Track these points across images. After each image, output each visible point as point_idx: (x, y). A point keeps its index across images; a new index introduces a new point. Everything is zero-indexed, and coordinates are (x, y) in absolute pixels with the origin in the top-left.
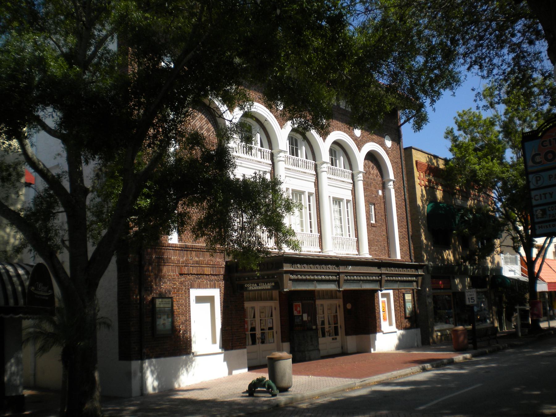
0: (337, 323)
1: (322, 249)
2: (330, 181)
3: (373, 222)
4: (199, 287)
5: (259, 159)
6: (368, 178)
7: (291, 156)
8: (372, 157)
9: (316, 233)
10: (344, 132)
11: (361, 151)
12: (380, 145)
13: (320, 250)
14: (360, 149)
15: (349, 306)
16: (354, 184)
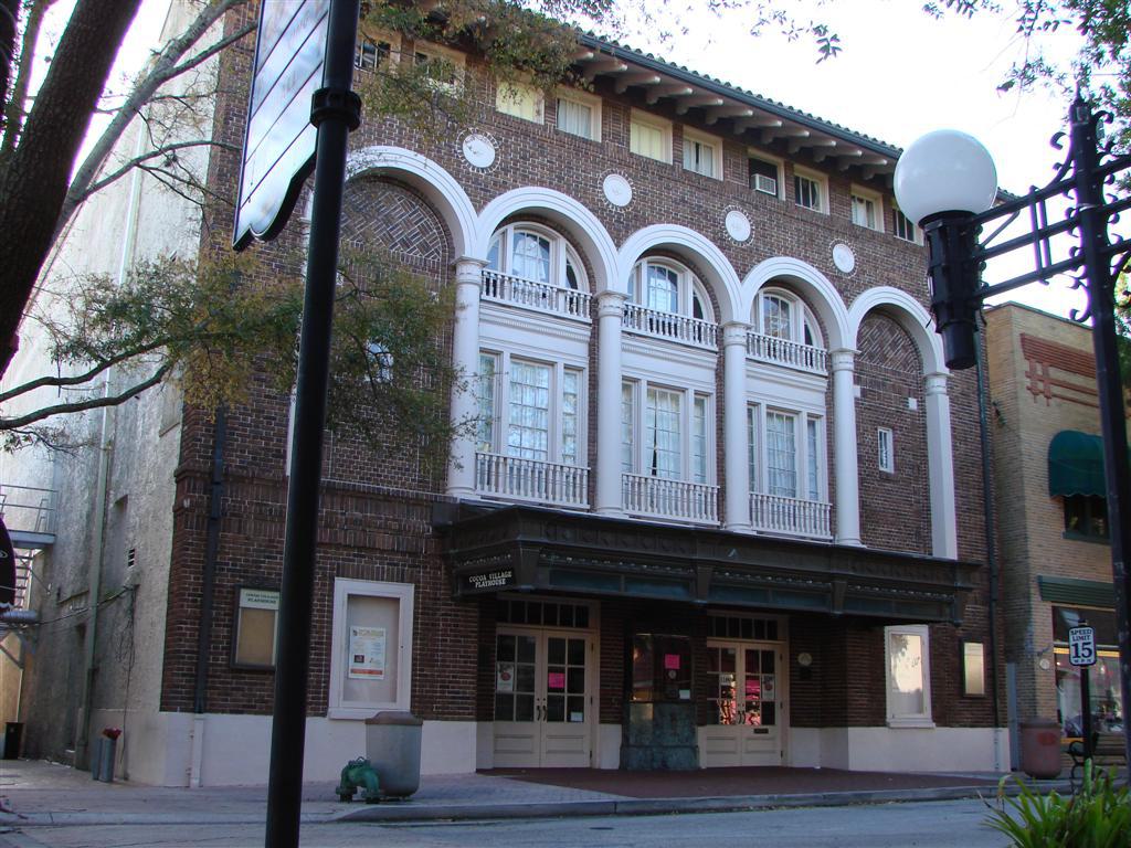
0: (581, 690)
3: (888, 466)
4: (358, 575)
10: (806, 259)
11: (481, 215)
14: (848, 301)
16: (831, 378)
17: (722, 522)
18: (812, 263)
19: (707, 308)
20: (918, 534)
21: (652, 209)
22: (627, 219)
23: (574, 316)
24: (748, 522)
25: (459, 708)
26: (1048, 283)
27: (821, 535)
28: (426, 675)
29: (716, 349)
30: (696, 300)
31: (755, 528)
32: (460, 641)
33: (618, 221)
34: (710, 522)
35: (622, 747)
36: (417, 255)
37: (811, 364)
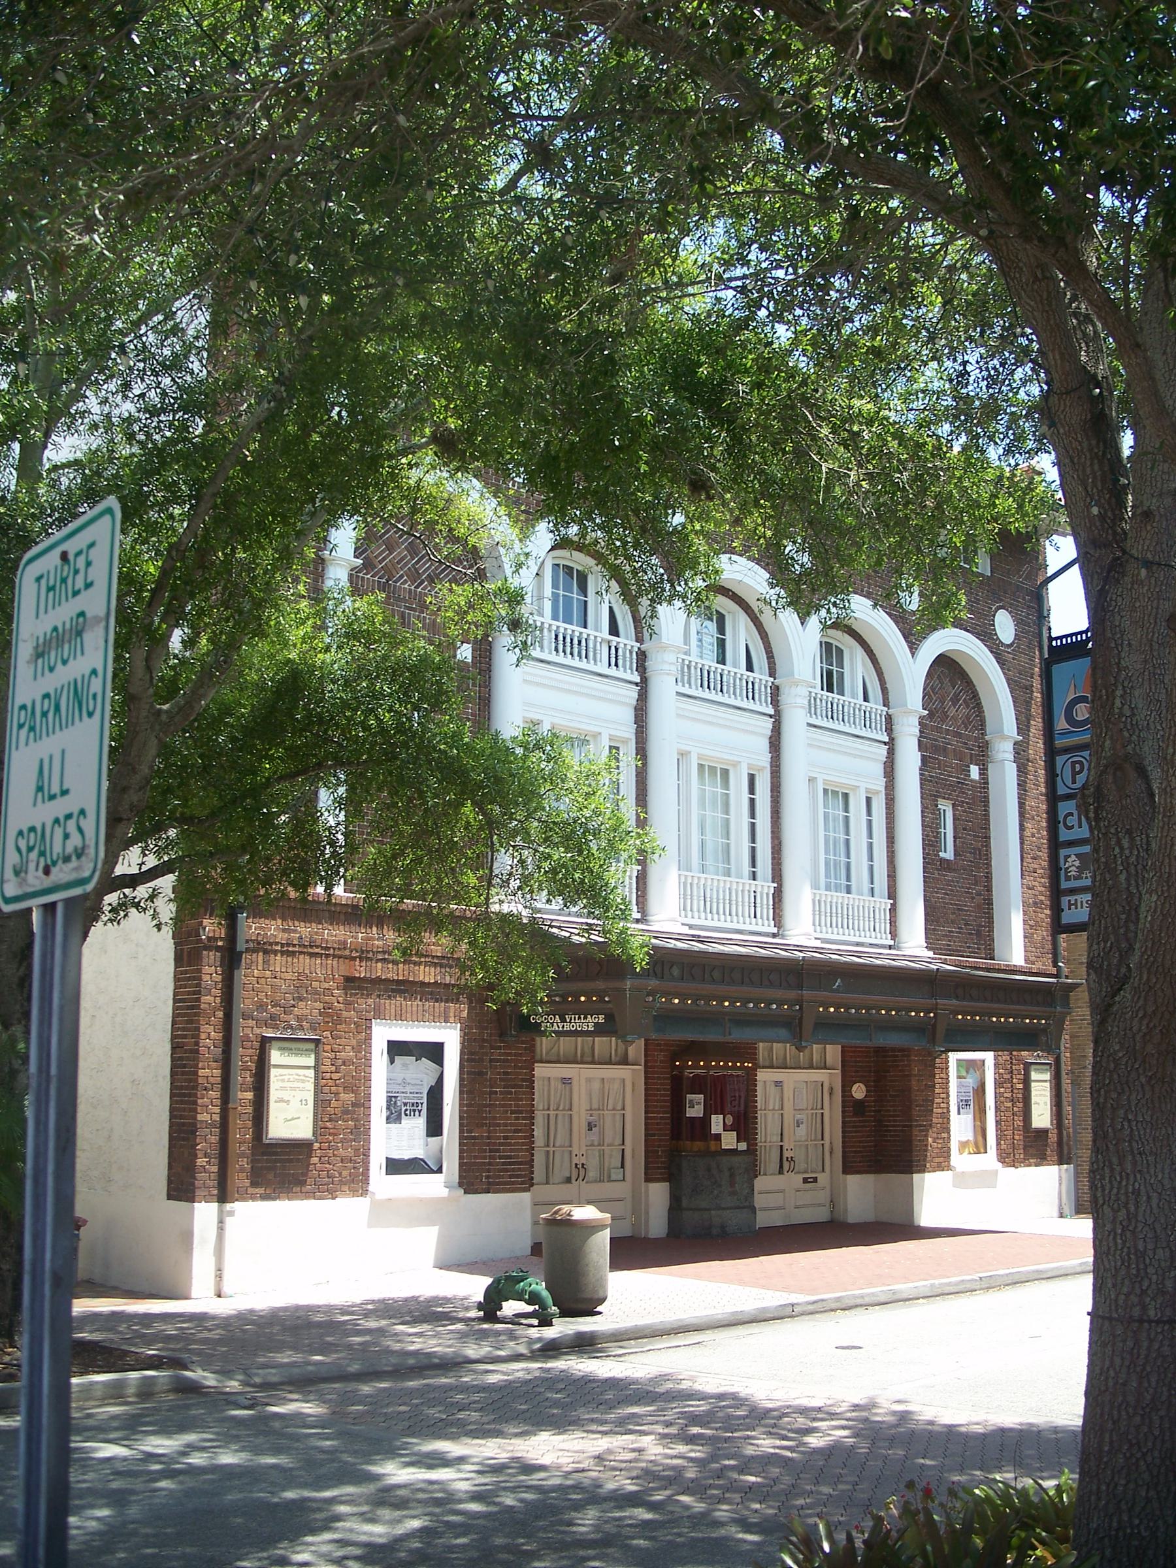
1: (894, 934)
3: (948, 854)
4: (400, 1017)
5: (602, 668)
7: (825, 693)
8: (947, 669)
9: (766, 887)
12: (978, 635)
14: (913, 648)
15: (859, 1091)
16: (891, 745)
19: (760, 659)
20: (979, 934)
23: (750, 705)
24: (811, 929)
25: (511, 1177)
28: (474, 1138)
35: (671, 1209)
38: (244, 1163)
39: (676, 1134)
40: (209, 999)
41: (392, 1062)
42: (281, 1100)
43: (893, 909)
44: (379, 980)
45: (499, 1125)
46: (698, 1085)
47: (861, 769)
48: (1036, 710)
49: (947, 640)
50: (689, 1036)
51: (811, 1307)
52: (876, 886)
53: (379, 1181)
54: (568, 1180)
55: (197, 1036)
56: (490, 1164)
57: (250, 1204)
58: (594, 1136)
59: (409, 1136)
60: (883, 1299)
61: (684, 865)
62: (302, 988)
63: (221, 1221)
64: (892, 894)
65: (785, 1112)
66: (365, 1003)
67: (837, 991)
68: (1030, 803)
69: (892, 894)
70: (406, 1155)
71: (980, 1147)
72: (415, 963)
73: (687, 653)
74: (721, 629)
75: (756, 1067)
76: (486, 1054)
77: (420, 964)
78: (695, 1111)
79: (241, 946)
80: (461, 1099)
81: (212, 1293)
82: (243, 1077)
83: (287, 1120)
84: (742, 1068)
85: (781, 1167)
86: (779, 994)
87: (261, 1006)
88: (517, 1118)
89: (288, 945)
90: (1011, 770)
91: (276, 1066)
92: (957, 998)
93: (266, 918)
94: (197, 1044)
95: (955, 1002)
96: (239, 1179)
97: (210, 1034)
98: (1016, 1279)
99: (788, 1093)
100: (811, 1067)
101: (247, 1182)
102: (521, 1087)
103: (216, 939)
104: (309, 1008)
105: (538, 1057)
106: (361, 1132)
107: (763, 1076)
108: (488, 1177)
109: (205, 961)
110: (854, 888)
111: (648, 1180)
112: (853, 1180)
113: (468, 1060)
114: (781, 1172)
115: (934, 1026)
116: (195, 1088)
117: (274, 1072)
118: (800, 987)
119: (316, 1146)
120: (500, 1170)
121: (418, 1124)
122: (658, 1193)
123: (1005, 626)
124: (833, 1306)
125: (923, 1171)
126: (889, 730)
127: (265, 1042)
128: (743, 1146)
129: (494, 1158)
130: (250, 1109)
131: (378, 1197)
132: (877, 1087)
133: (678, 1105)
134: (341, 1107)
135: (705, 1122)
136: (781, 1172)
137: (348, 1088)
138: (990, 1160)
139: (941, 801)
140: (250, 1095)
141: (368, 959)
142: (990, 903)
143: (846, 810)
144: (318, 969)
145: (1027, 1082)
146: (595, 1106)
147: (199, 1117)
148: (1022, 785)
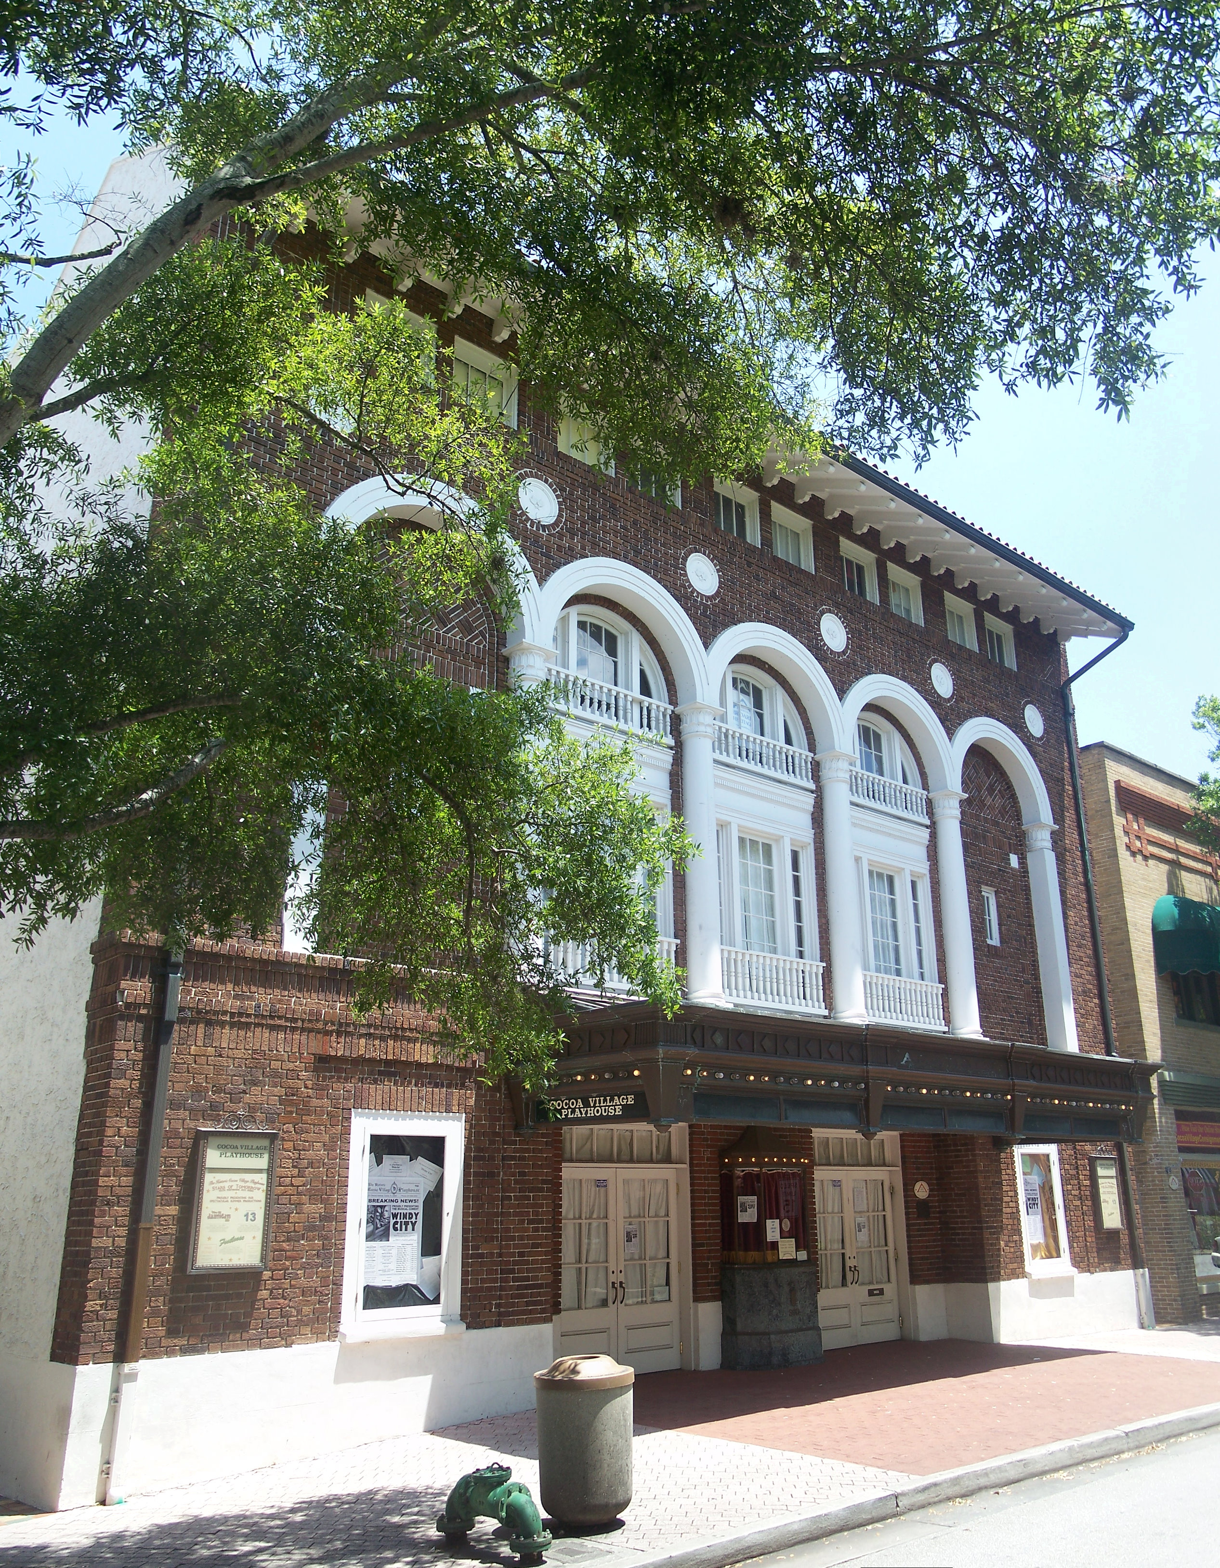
2: (859, 813)
3: (994, 940)
4: (388, 1105)
6: (977, 817)
8: (980, 758)
12: (1010, 726)
13: (826, 1013)
14: (950, 733)
15: (922, 1190)
17: (830, 1010)
18: (912, 684)
20: (1030, 1022)
21: (742, 603)
22: (713, 612)
23: (791, 779)
24: (864, 1011)
25: (528, 1304)
26: (1213, 760)
27: (935, 1026)
28: (481, 1256)
29: (813, 787)
30: (642, 674)
31: (731, 999)
32: (528, 1198)
33: (704, 614)
34: (810, 1010)
35: (724, 1334)
36: (456, 636)
37: (649, 726)
38: (160, 1303)
39: (727, 1243)
40: (123, 1083)
41: (379, 1161)
42: (219, 1215)
43: (945, 994)
44: (360, 1061)
45: (513, 1238)
46: (750, 1185)
47: (906, 853)
48: (1068, 802)
49: (979, 728)
50: (740, 1119)
51: (921, 1498)
52: (926, 970)
53: (357, 1321)
54: (604, 1303)
55: (101, 1133)
56: (501, 1288)
57: (165, 1360)
58: (634, 1248)
59: (398, 1259)
60: (1012, 1474)
61: (726, 939)
62: (257, 1068)
63: (116, 1390)
64: (943, 978)
65: (845, 1215)
66: (340, 1089)
67: (905, 1067)
68: (1071, 892)
69: (943, 978)
70: (395, 1281)
71: (1052, 1252)
72: (409, 1040)
73: (723, 718)
74: (758, 704)
75: (812, 1164)
76: (498, 1150)
77: (415, 1040)
78: (748, 1216)
79: (171, 1014)
80: (466, 1207)
81: (92, 1499)
82: (163, 1185)
83: (224, 1242)
84: (798, 1164)
85: (844, 1277)
86: (842, 1069)
87: (198, 1092)
88: (536, 1230)
89: (240, 1014)
90: (1050, 858)
91: (213, 1170)
92: (1034, 1078)
93: (212, 981)
94: (101, 1142)
95: (1032, 1082)
96: (149, 1326)
97: (120, 1129)
98: (1168, 1431)
99: (847, 1194)
100: (870, 1164)
101: (162, 1331)
102: (541, 1190)
103: (138, 1006)
104: (267, 1095)
105: (567, 1155)
106: (332, 1254)
107: (821, 1174)
108: (498, 1306)
109: (120, 1034)
110: (904, 971)
111: (696, 1299)
112: (922, 1292)
113: (476, 1158)
114: (844, 1284)
115: (1012, 1110)
116: (93, 1203)
117: (208, 1177)
118: (864, 1061)
119: (267, 1274)
120: (513, 1297)
121: (413, 1240)
122: (709, 1315)
123: (1034, 721)
124: (950, 1492)
125: (997, 1278)
126: (930, 813)
127: (199, 1140)
128: (803, 1256)
129: (506, 1280)
130: (173, 1229)
131: (349, 1340)
132: (939, 1185)
133: (728, 1210)
134: (304, 1227)
135: (759, 1228)
136: (844, 1284)
137: (316, 1196)
138: (1063, 1266)
139: (984, 888)
140: (173, 1210)
141: (348, 1034)
142: (1039, 992)
143: (892, 892)
144: (279, 1044)
145: (1093, 1178)
146: (635, 1212)
147: (95, 1243)
148: (1061, 874)
